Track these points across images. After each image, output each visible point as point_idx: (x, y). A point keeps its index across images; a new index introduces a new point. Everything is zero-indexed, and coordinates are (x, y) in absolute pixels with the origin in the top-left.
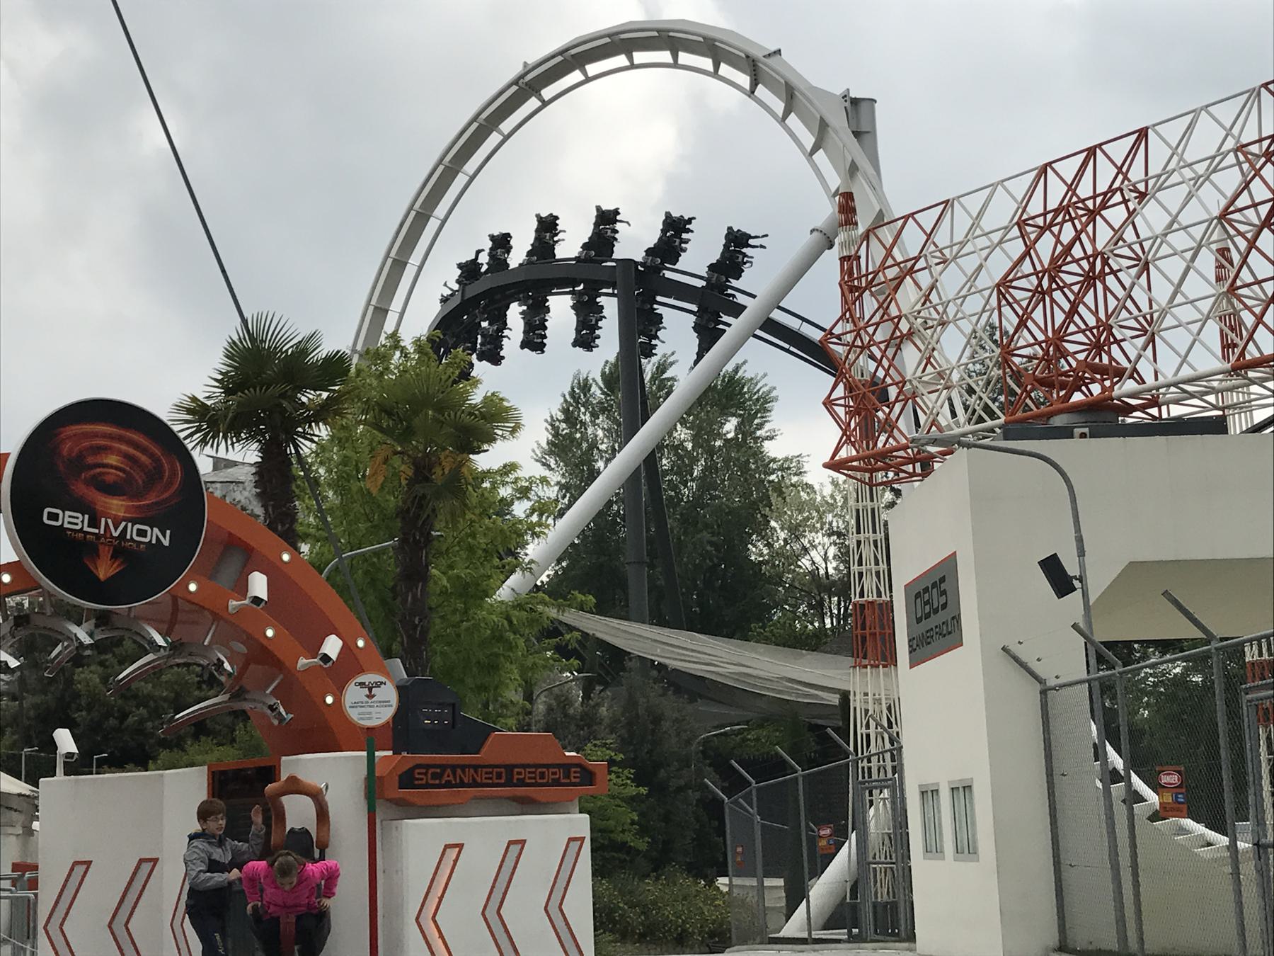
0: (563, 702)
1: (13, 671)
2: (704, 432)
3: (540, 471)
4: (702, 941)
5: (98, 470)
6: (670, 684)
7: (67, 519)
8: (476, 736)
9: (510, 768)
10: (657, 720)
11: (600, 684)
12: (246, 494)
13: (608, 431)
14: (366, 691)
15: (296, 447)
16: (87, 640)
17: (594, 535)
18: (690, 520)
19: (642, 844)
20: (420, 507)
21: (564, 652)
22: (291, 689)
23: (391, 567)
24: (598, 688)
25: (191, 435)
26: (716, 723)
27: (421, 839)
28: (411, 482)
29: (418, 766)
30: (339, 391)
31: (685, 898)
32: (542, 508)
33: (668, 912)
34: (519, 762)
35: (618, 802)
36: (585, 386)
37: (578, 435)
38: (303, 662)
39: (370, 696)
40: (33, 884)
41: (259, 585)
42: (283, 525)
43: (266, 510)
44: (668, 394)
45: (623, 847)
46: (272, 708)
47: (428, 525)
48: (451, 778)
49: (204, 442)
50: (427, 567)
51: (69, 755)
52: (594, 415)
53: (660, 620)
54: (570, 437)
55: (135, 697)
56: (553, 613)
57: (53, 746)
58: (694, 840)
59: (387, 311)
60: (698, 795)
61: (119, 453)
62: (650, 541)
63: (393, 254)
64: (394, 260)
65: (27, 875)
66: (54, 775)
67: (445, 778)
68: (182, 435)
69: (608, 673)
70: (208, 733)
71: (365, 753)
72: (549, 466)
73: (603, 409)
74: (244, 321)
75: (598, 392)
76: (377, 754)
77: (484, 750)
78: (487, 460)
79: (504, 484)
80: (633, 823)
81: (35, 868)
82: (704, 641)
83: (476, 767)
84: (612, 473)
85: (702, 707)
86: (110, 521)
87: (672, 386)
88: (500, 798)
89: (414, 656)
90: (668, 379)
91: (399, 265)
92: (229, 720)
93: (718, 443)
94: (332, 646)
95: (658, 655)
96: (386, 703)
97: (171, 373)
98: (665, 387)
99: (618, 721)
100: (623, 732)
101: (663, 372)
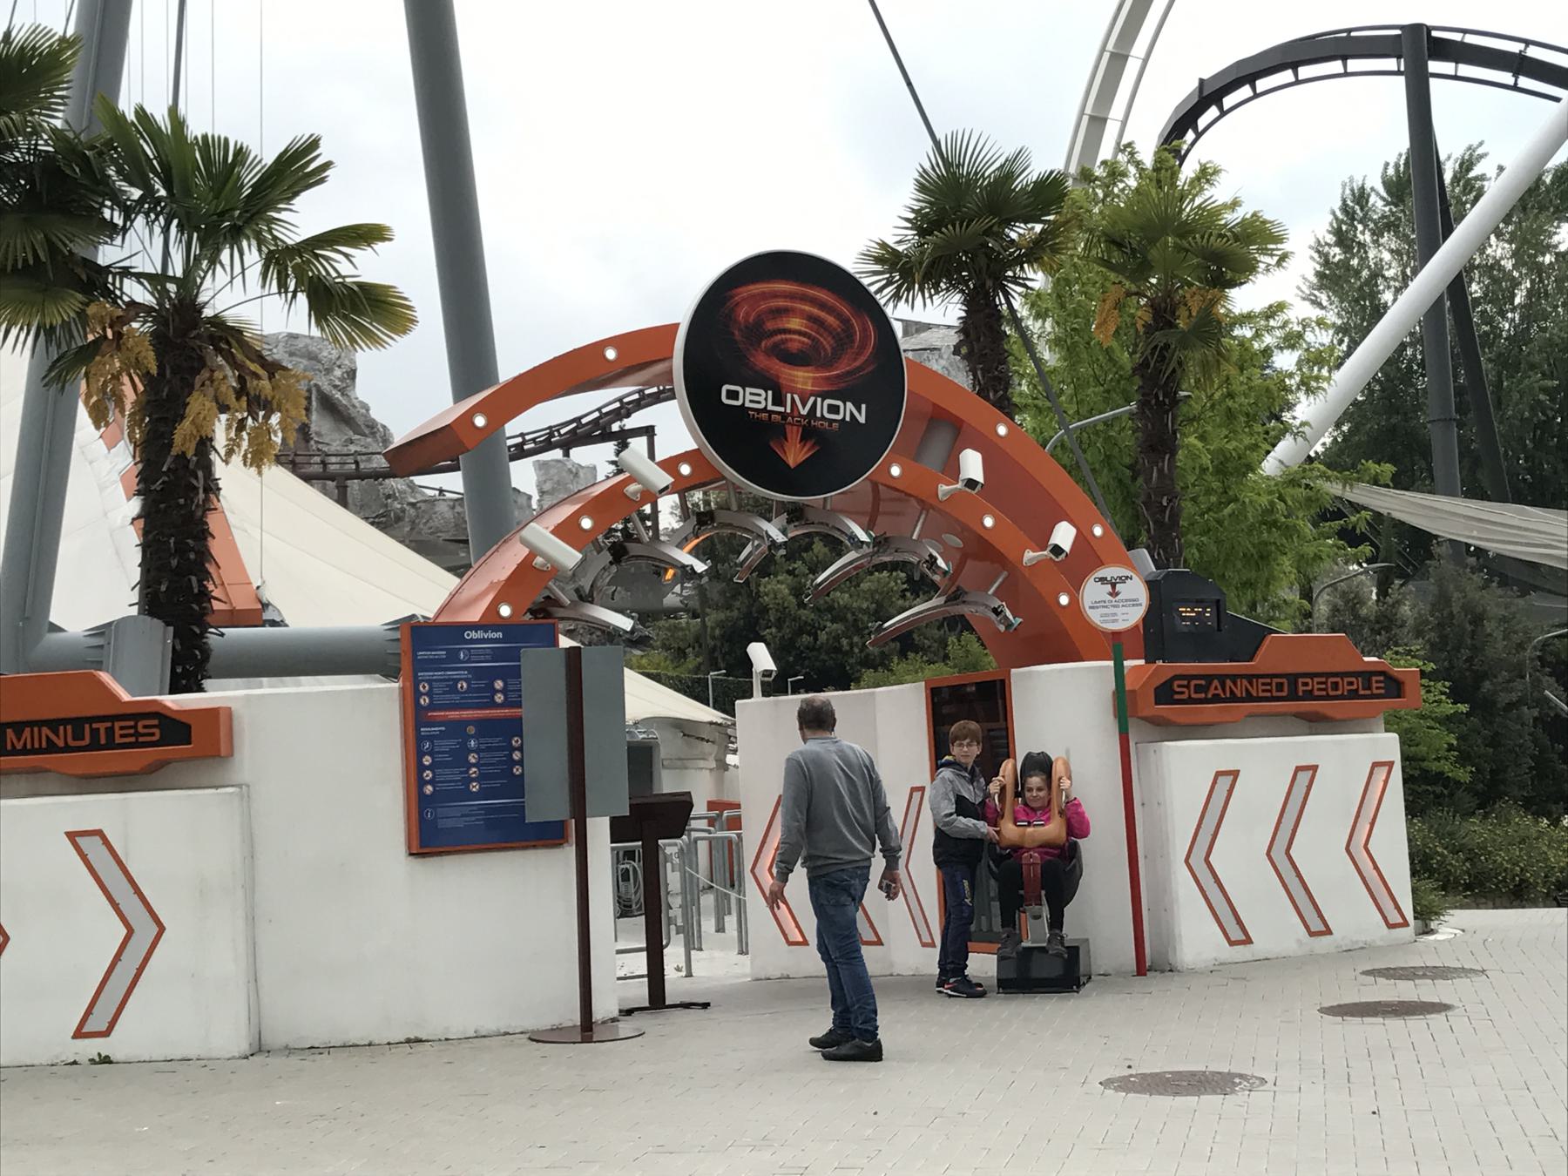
0: (1353, 601)
1: (701, 576)
2: (1529, 243)
3: (1314, 313)
4: (1548, 894)
8: (1250, 639)
9: (1293, 678)
10: (1478, 619)
11: (1398, 577)
12: (943, 362)
13: (1396, 253)
14: (1109, 588)
15: (1007, 295)
16: (780, 538)
17: (1383, 390)
18: (1510, 362)
19: (1463, 775)
20: (1162, 358)
21: (1351, 537)
22: (1017, 588)
23: (1128, 440)
24: (1397, 582)
26: (1557, 621)
27: (1185, 765)
29: (1176, 678)
30: (1054, 222)
32: (1317, 359)
33: (1501, 857)
35: (1430, 723)
36: (1361, 197)
37: (1355, 262)
38: (1029, 555)
39: (1114, 594)
40: (735, 823)
41: (972, 464)
42: (996, 392)
43: (975, 376)
45: (1440, 777)
46: (996, 611)
48: (1220, 691)
49: (897, 297)
50: (1174, 433)
51: (767, 673)
52: (1377, 233)
53: (1475, 491)
54: (1345, 264)
55: (830, 609)
56: (1335, 488)
57: (748, 664)
59: (1105, 120)
62: (1460, 391)
63: (1110, 47)
64: (1112, 54)
66: (751, 696)
68: (872, 289)
69: (1408, 563)
70: (917, 649)
71: (1111, 663)
74: (937, 143)
75: (1380, 204)
76: (1126, 663)
77: (1258, 658)
78: (1243, 299)
79: (1269, 330)
80: (1451, 748)
81: (738, 806)
83: (1250, 678)
84: (1403, 308)
85: (1537, 600)
87: (1482, 187)
88: (1284, 714)
89: (1164, 544)
90: (1476, 178)
92: (936, 633)
93: (1548, 259)
94: (1064, 535)
95: (1473, 536)
96: (1135, 603)
97: (857, 216)
99: (1427, 622)
101: (1469, 169)
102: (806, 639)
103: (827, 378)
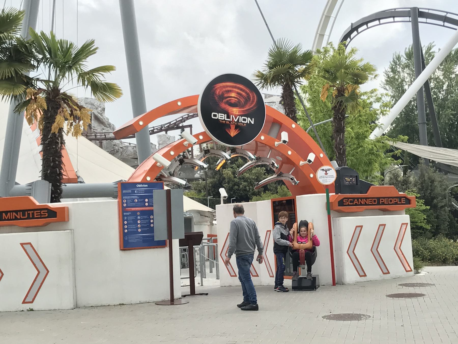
0: (396, 176)
2: (447, 72)
3: (385, 92)
4: (453, 262)
5: (228, 99)
6: (436, 168)
7: (220, 116)
8: (366, 187)
9: (379, 199)
10: (432, 182)
11: (410, 169)
12: (276, 106)
13: (409, 74)
14: (325, 172)
15: (295, 86)
16: (229, 158)
17: (405, 114)
18: (442, 107)
19: (428, 227)
20: (340, 105)
21: (395, 157)
22: (298, 172)
23: (331, 129)
24: (409, 170)
25: (258, 85)
27: (347, 224)
28: (337, 97)
31: (445, 246)
33: (439, 251)
34: (382, 196)
36: (399, 58)
38: (302, 163)
39: (326, 174)
40: (216, 241)
41: (285, 136)
42: (292, 115)
44: (432, 58)
46: (292, 179)
47: (344, 111)
48: (357, 202)
49: (263, 87)
51: (225, 197)
52: (403, 68)
53: (431, 144)
54: (394, 78)
55: (243, 178)
56: (391, 143)
57: (219, 194)
58: (448, 225)
60: (449, 209)
61: (235, 92)
62: (427, 115)
65: (213, 238)
66: (220, 204)
67: (355, 203)
68: (256, 85)
69: (412, 165)
71: (325, 194)
72: (386, 89)
73: (407, 66)
74: (275, 42)
78: (362, 88)
80: (425, 219)
81: (216, 236)
82: (450, 151)
83: (366, 198)
84: (412, 90)
85: (450, 176)
86: (233, 116)
89: (341, 159)
90: (432, 52)
91: (328, 17)
92: (274, 186)
93: (453, 76)
94: (312, 157)
95: (431, 157)
96: (332, 176)
97: (252, 64)
98: (431, 56)
99: (417, 182)
100: (419, 186)
101: (430, 50)
102: (236, 187)
103: (243, 111)
